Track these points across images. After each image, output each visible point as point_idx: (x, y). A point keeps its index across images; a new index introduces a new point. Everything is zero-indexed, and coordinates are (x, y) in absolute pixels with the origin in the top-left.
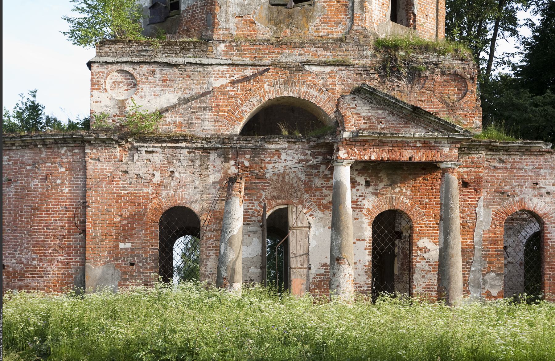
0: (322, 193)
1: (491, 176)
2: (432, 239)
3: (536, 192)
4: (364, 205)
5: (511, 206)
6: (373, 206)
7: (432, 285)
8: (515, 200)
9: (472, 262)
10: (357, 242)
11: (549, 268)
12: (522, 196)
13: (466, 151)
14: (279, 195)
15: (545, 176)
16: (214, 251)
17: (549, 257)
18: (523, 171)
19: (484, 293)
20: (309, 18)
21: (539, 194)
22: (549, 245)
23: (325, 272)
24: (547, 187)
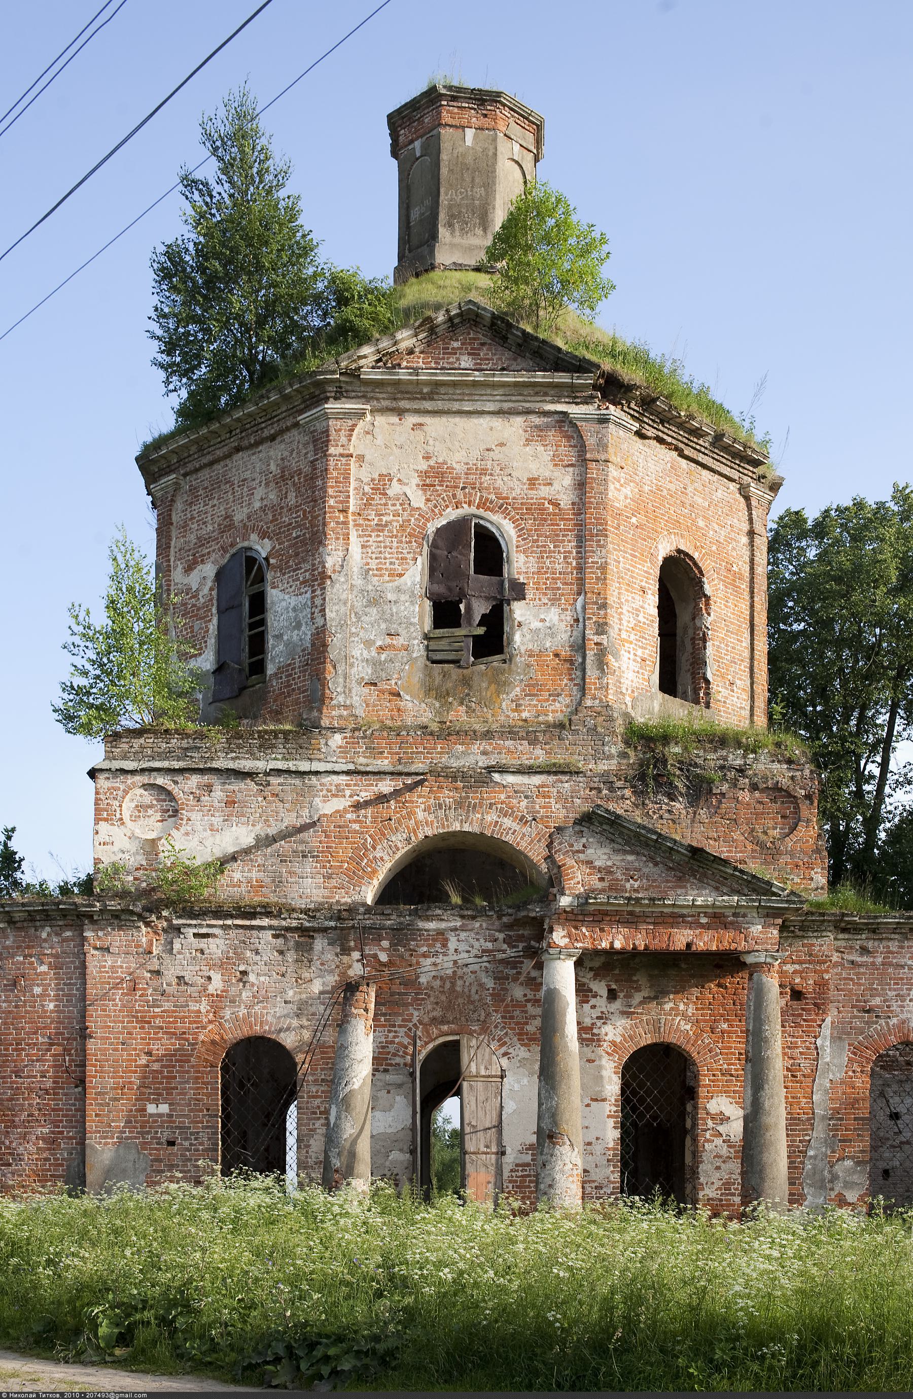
0: (526, 1012)
1: (845, 979)
2: (734, 1098)
4: (606, 1034)
8: (891, 1023)
10: (593, 1104)
14: (444, 1016)
20: (501, 685)
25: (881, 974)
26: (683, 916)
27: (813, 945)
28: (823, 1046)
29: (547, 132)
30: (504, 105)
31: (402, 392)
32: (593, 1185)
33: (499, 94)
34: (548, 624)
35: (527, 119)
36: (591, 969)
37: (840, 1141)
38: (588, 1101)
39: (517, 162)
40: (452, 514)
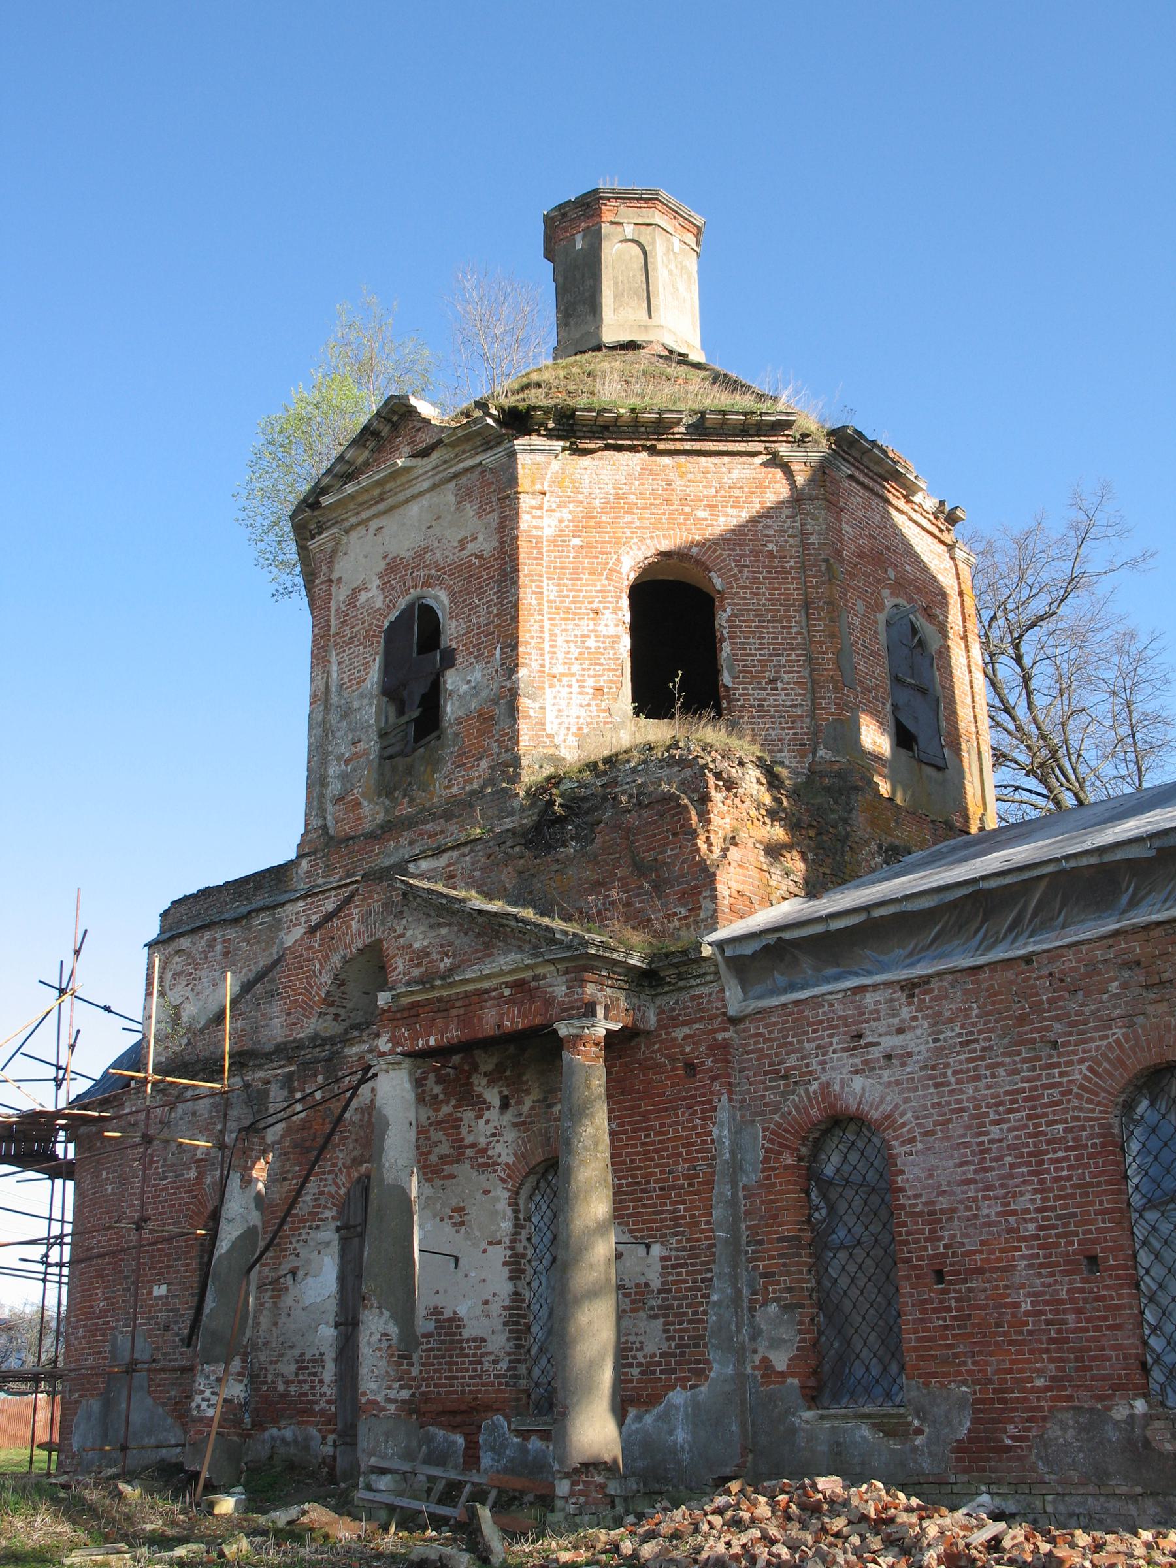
0: (428, 1139)
1: (754, 1035)
2: (627, 1224)
3: (858, 1061)
4: (500, 1156)
5: (800, 1104)
6: (515, 1155)
7: (631, 1349)
8: (811, 1090)
9: (711, 1279)
10: (490, 1248)
11: (908, 1278)
12: (824, 1079)
13: (682, 984)
14: (362, 1155)
15: (877, 1011)
16: (269, 1293)
17: (906, 1242)
18: (826, 1008)
19: (757, 1363)
20: (435, 763)
21: (865, 1062)
22: (903, 1207)
23: (436, 1328)
24: (882, 1040)
25: (795, 1020)
26: (487, 991)
27: (700, 996)
28: (720, 1137)
30: (609, 199)
31: (360, 505)
32: (491, 1358)
33: (596, 191)
34: (473, 684)
35: (641, 199)
36: (486, 1074)
37: (763, 1275)
38: (484, 1245)
39: (633, 241)
40: (403, 603)
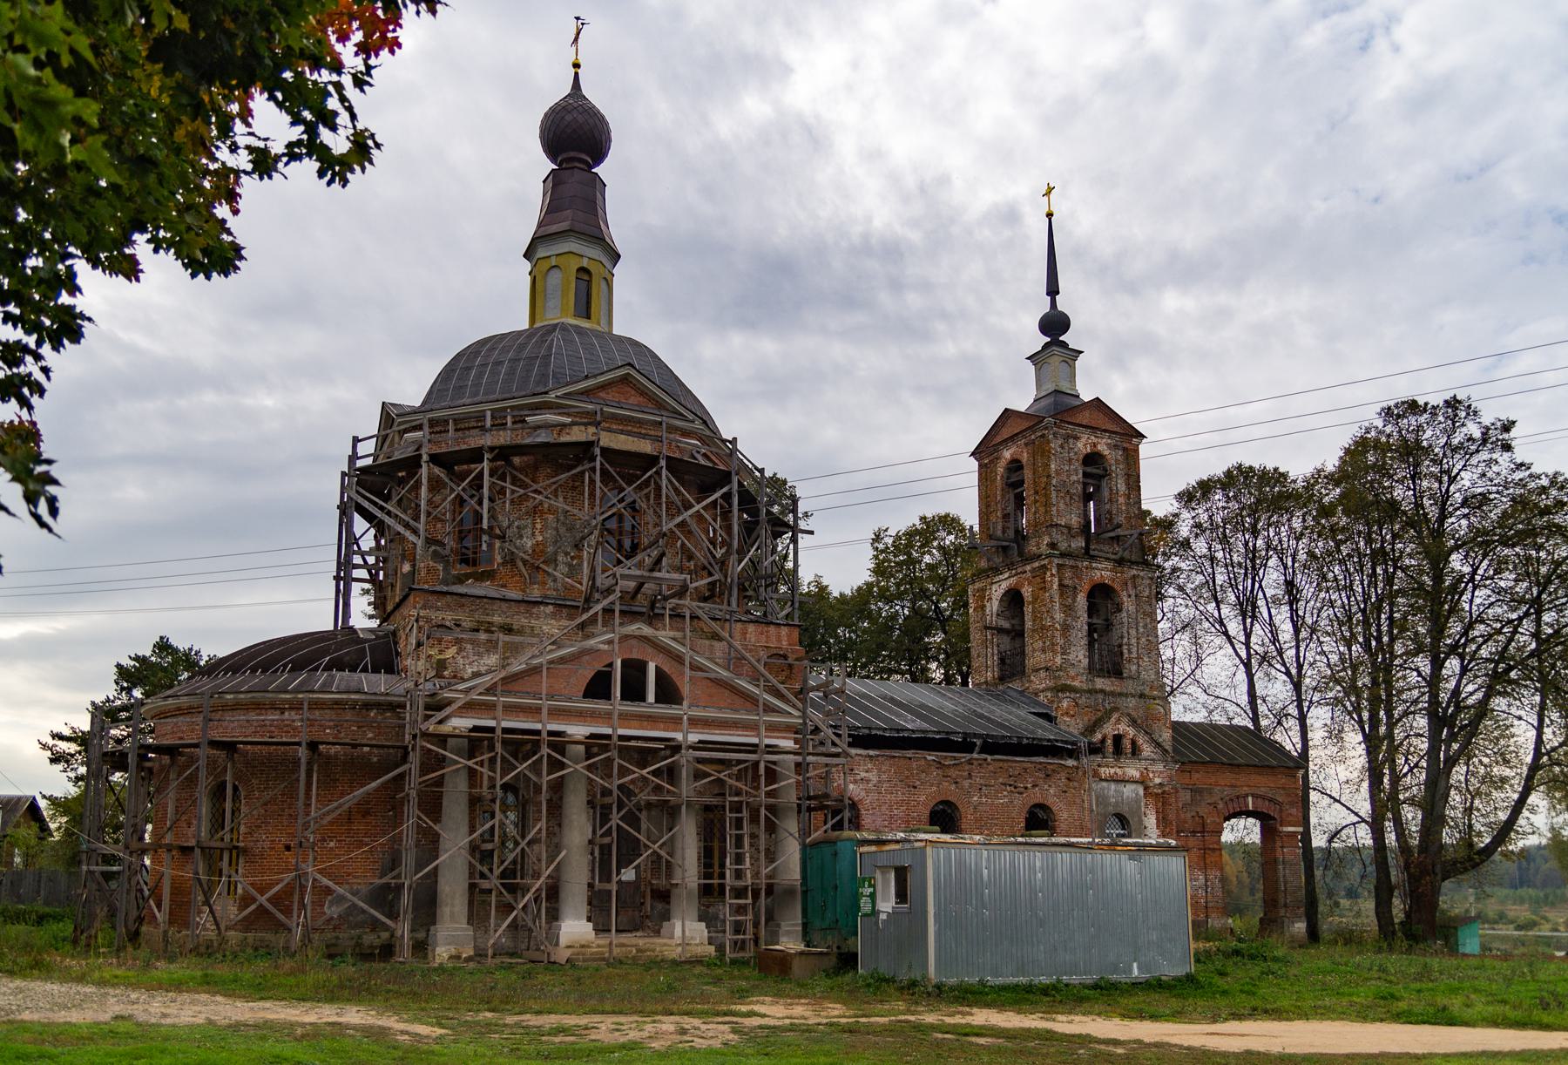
29: (60, 504)
